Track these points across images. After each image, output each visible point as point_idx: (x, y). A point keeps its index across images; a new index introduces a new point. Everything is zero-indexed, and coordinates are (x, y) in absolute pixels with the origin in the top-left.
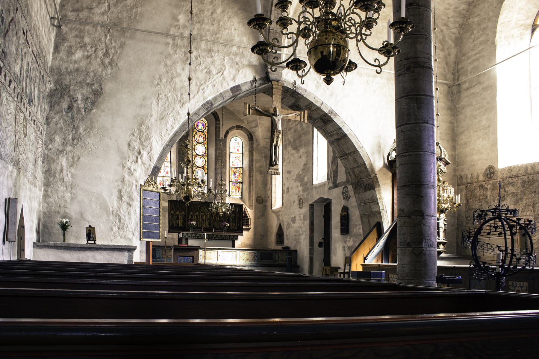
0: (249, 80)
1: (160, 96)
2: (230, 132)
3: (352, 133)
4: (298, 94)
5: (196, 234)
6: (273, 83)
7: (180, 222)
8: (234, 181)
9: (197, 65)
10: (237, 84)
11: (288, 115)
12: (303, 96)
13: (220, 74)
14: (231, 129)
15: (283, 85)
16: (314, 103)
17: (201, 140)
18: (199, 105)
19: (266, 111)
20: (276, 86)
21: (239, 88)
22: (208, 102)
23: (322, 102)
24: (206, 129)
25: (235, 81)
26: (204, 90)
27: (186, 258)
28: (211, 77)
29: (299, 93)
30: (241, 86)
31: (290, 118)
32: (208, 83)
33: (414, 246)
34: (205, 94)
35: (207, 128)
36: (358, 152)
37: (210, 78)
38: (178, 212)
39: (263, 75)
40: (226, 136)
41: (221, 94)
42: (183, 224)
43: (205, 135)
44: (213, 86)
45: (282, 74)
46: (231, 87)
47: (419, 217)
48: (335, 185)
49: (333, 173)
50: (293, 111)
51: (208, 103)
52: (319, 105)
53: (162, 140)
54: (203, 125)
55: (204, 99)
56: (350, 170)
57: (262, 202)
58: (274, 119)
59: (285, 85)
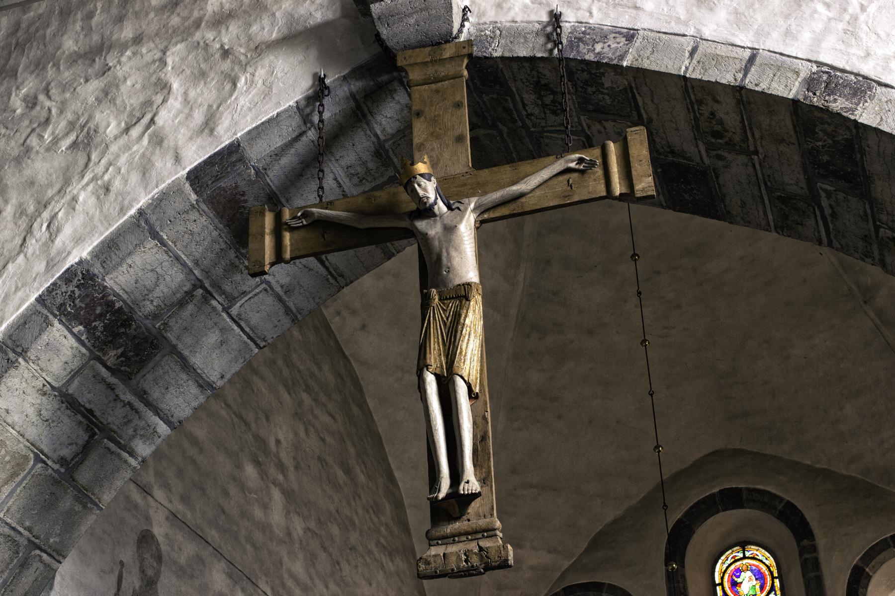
0: (292, 103)
9: (33, 130)
14: (874, 555)
18: (28, 296)
22: (68, 276)
23: (747, 54)
25: (212, 131)
26: (54, 227)
28: (94, 157)
32: (74, 188)
34: (58, 242)
35: (777, 583)
44: (101, 192)
54: (759, 576)
55: (50, 266)
56: (246, 198)
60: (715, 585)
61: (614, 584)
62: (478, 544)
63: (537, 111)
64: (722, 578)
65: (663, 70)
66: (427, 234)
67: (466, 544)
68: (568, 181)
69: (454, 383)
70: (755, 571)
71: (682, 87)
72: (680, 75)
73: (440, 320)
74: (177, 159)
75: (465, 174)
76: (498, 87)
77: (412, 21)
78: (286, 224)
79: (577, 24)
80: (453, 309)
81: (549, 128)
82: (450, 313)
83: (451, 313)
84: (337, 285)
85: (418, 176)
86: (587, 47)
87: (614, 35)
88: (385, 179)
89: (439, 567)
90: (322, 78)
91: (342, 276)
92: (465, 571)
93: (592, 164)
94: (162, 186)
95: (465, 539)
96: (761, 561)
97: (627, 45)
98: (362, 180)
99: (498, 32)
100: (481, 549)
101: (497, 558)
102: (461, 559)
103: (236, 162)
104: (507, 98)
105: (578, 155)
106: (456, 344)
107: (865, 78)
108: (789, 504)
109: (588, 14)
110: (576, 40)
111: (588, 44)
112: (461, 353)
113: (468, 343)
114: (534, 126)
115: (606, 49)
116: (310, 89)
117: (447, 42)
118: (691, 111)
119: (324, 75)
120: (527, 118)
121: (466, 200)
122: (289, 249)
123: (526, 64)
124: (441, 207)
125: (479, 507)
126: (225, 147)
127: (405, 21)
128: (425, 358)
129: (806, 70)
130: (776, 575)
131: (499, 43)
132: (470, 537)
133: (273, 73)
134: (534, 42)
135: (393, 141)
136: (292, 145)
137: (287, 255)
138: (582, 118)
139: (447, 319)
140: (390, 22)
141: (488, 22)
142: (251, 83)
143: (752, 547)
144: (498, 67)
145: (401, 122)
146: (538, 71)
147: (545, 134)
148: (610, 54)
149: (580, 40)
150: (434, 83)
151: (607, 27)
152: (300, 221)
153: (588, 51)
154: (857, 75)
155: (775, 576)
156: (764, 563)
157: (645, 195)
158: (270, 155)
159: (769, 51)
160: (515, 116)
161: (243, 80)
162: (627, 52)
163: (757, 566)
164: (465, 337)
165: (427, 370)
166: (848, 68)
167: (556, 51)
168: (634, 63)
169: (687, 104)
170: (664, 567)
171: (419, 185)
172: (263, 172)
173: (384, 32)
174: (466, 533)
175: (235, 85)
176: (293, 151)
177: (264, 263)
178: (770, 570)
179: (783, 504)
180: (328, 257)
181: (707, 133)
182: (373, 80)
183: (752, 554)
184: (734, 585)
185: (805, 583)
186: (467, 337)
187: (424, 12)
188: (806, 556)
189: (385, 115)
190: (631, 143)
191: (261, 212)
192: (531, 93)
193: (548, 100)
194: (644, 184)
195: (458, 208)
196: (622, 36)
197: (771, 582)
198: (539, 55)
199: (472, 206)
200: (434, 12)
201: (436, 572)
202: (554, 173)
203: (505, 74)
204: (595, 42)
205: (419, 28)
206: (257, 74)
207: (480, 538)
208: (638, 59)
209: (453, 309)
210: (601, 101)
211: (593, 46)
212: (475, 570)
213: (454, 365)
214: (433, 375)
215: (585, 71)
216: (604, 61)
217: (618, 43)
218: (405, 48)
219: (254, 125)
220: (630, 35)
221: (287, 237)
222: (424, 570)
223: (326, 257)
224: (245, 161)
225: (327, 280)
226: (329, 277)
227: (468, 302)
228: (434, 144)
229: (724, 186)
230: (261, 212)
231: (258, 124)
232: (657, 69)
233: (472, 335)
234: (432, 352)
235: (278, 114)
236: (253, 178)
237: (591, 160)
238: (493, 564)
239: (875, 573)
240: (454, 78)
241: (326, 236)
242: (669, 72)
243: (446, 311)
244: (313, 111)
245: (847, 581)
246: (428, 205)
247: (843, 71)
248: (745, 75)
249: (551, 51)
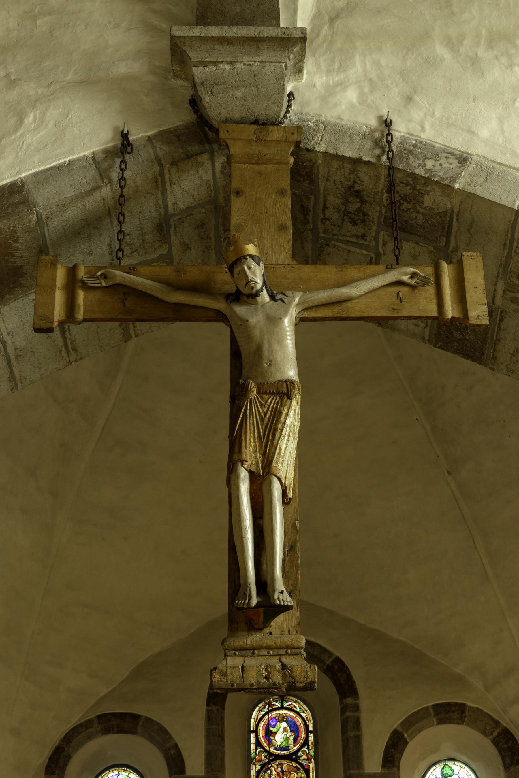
2: (413, 736)
21: (16, 199)
24: (306, 742)
35: (311, 737)
54: (294, 728)
56: (17, 245)
58: (239, 318)
61: (152, 717)
62: (280, 661)
63: (335, 217)
64: (257, 726)
65: (496, 200)
66: (247, 321)
67: (267, 659)
68: (398, 294)
69: (270, 484)
70: (291, 723)
71: (510, 221)
72: (513, 209)
73: (257, 414)
75: (286, 266)
76: (306, 184)
77: (239, 94)
78: (83, 282)
79: (407, 136)
80: (272, 405)
81: (340, 237)
82: (268, 409)
83: (270, 409)
84: (68, 359)
85: (248, 257)
86: (417, 162)
87: (446, 155)
88: (156, 255)
89: (236, 680)
90: (126, 134)
91: (75, 350)
92: (265, 688)
95: (266, 653)
96: (298, 713)
97: (460, 167)
98: (134, 252)
99: (322, 126)
100: (284, 667)
101: (302, 679)
102: (261, 675)
103: (18, 203)
104: (311, 196)
105: (412, 270)
106: (275, 443)
108: (338, 661)
109: (420, 128)
110: (406, 152)
111: (418, 159)
112: (280, 453)
113: (287, 444)
114: (325, 231)
115: (438, 168)
116: (110, 142)
117: (273, 124)
118: (507, 247)
119: (128, 131)
120: (322, 221)
121: (290, 293)
122: (82, 309)
123: (348, 166)
124: (265, 296)
125: (283, 620)
126: (6, 185)
127: (232, 92)
128: (240, 452)
130: (311, 728)
131: (322, 138)
132: (271, 652)
133: (67, 116)
134: (360, 145)
135: (179, 217)
136: (83, 198)
137: (80, 316)
138: (382, 233)
139: (265, 414)
140: (214, 90)
141: (311, 114)
142: (41, 122)
143: (291, 698)
144: (316, 162)
145: (194, 199)
146: (357, 176)
147: (333, 242)
148: (442, 173)
149: (410, 152)
150: (257, 164)
151: (439, 145)
152: (99, 281)
153: (419, 166)
155: (310, 729)
156: (301, 716)
157: (479, 323)
158: (57, 203)
160: (310, 218)
161: (31, 117)
162: (459, 174)
163: (293, 718)
164: (284, 437)
165: (242, 465)
167: (384, 158)
168: (467, 187)
169: (506, 240)
170: (205, 707)
171: (249, 268)
172: (44, 220)
173: (207, 99)
174: (269, 648)
175: (21, 121)
176: (81, 205)
177: (53, 320)
178: (305, 724)
179: (331, 659)
180: (71, 328)
181: (514, 273)
182: (182, 148)
183: (289, 705)
184: (269, 734)
185: (343, 741)
186: (286, 437)
187: (253, 88)
188: (348, 714)
189: (183, 187)
190: (466, 268)
191: (52, 263)
192: (338, 197)
193: (352, 208)
194: (478, 312)
195: (282, 300)
196: (454, 157)
197: (305, 735)
198: (366, 159)
199: (297, 300)
200: (264, 90)
201: (232, 685)
202: (386, 283)
203: (320, 171)
204: (425, 158)
205: (245, 103)
206: (48, 114)
207: (283, 655)
208: (470, 184)
209: (272, 405)
210: (411, 220)
211: (423, 161)
212: (277, 688)
213: (273, 465)
214: (247, 472)
215: (410, 185)
216: (435, 179)
217: (451, 164)
218: (227, 121)
219: (42, 168)
221: (81, 296)
222: (219, 681)
223: (69, 327)
224: (29, 205)
225: (60, 351)
226: (63, 348)
227: (289, 401)
228: (254, 228)
229: (504, 330)
230: (52, 263)
231: (46, 167)
232: (490, 198)
233: (292, 436)
234: (248, 447)
235: (70, 162)
236: (33, 224)
237: (424, 276)
238: (298, 685)
239: (411, 739)
240: (280, 163)
241: (127, 303)
242: (503, 204)
243: (264, 406)
244: (111, 166)
245: (385, 745)
246: (254, 291)
249: (379, 157)
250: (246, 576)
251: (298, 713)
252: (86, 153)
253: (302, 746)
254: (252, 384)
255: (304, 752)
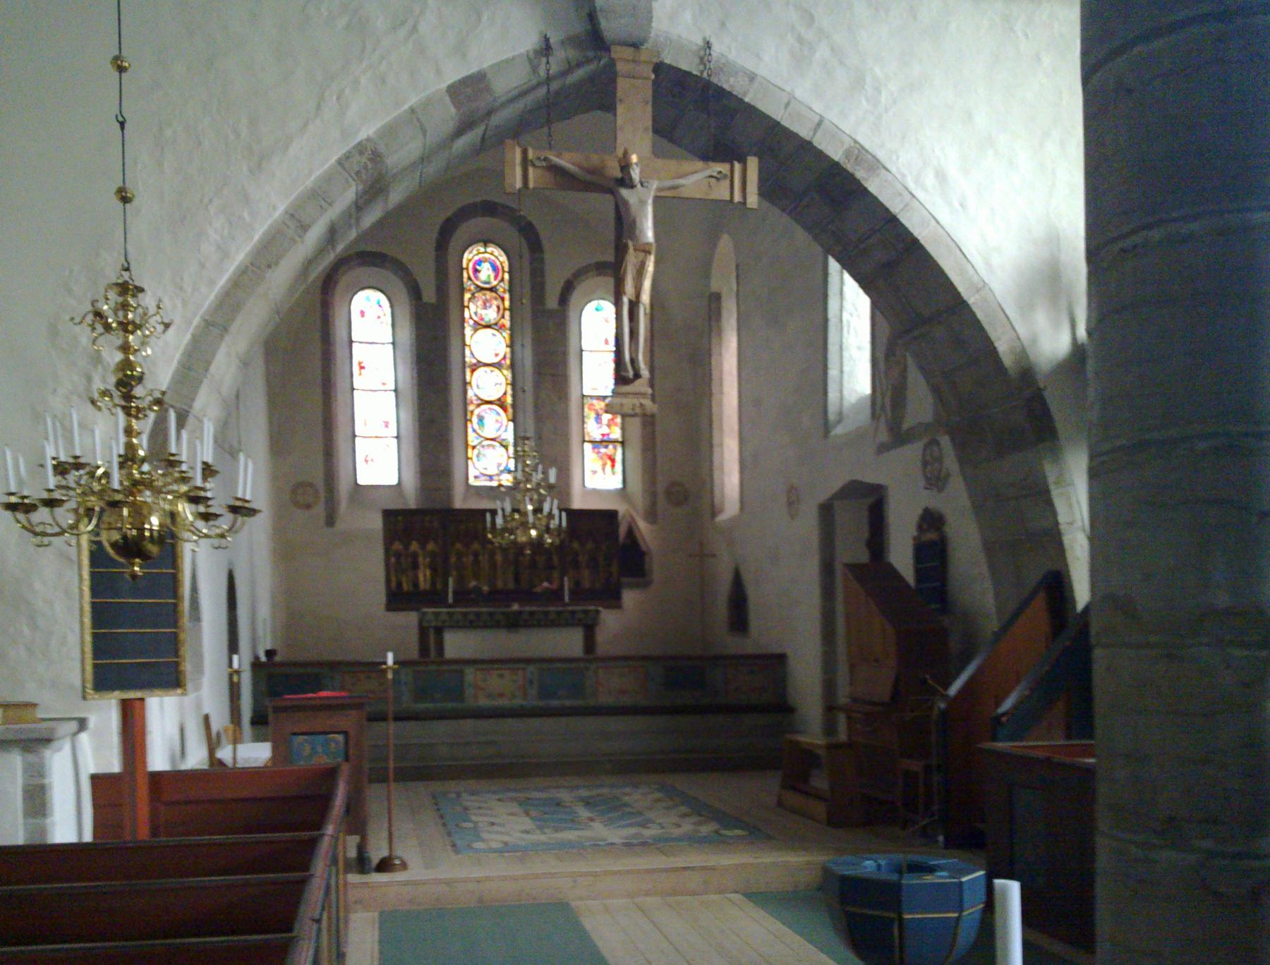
0: (523, 50)
1: (168, 133)
3: (941, 230)
4: (721, 93)
5: (465, 614)
6: (618, 52)
7: (424, 578)
8: (598, 438)
10: (473, 69)
11: (681, 181)
12: (741, 101)
13: (402, 33)
14: (579, 274)
15: (655, 60)
16: (785, 123)
17: (491, 315)
19: (592, 171)
20: (630, 67)
22: (360, 148)
23: (817, 119)
24: (502, 280)
25: (464, 55)
27: (320, 738)
29: (726, 87)
30: (489, 76)
31: (686, 193)
33: (1208, 844)
36: (968, 306)
37: (363, 51)
38: (414, 546)
39: (578, 27)
40: (564, 300)
41: (412, 110)
42: (433, 583)
43: (503, 299)
45: (650, 12)
46: (449, 82)
47: (1238, 652)
48: (899, 437)
49: (889, 393)
50: (700, 164)
51: (361, 153)
52: (804, 133)
53: (185, 303)
54: (495, 268)
57: (686, 498)
59: (667, 61)
60: (462, 269)
74: (439, 72)
78: (531, 161)
93: (725, 177)
94: (428, 92)
96: (497, 257)
99: (668, 42)
100: (641, 405)
107: (878, 160)
121: (651, 181)
129: (848, 142)
154: (874, 157)
156: (498, 259)
159: (830, 122)
166: (870, 150)
175: (479, 20)
184: (476, 271)
220: (752, 77)
221: (531, 170)
247: (867, 151)
248: (814, 134)
250: (624, 358)
251: (497, 257)
252: (522, 51)
253: (500, 281)
254: (630, 244)
255: (501, 287)
